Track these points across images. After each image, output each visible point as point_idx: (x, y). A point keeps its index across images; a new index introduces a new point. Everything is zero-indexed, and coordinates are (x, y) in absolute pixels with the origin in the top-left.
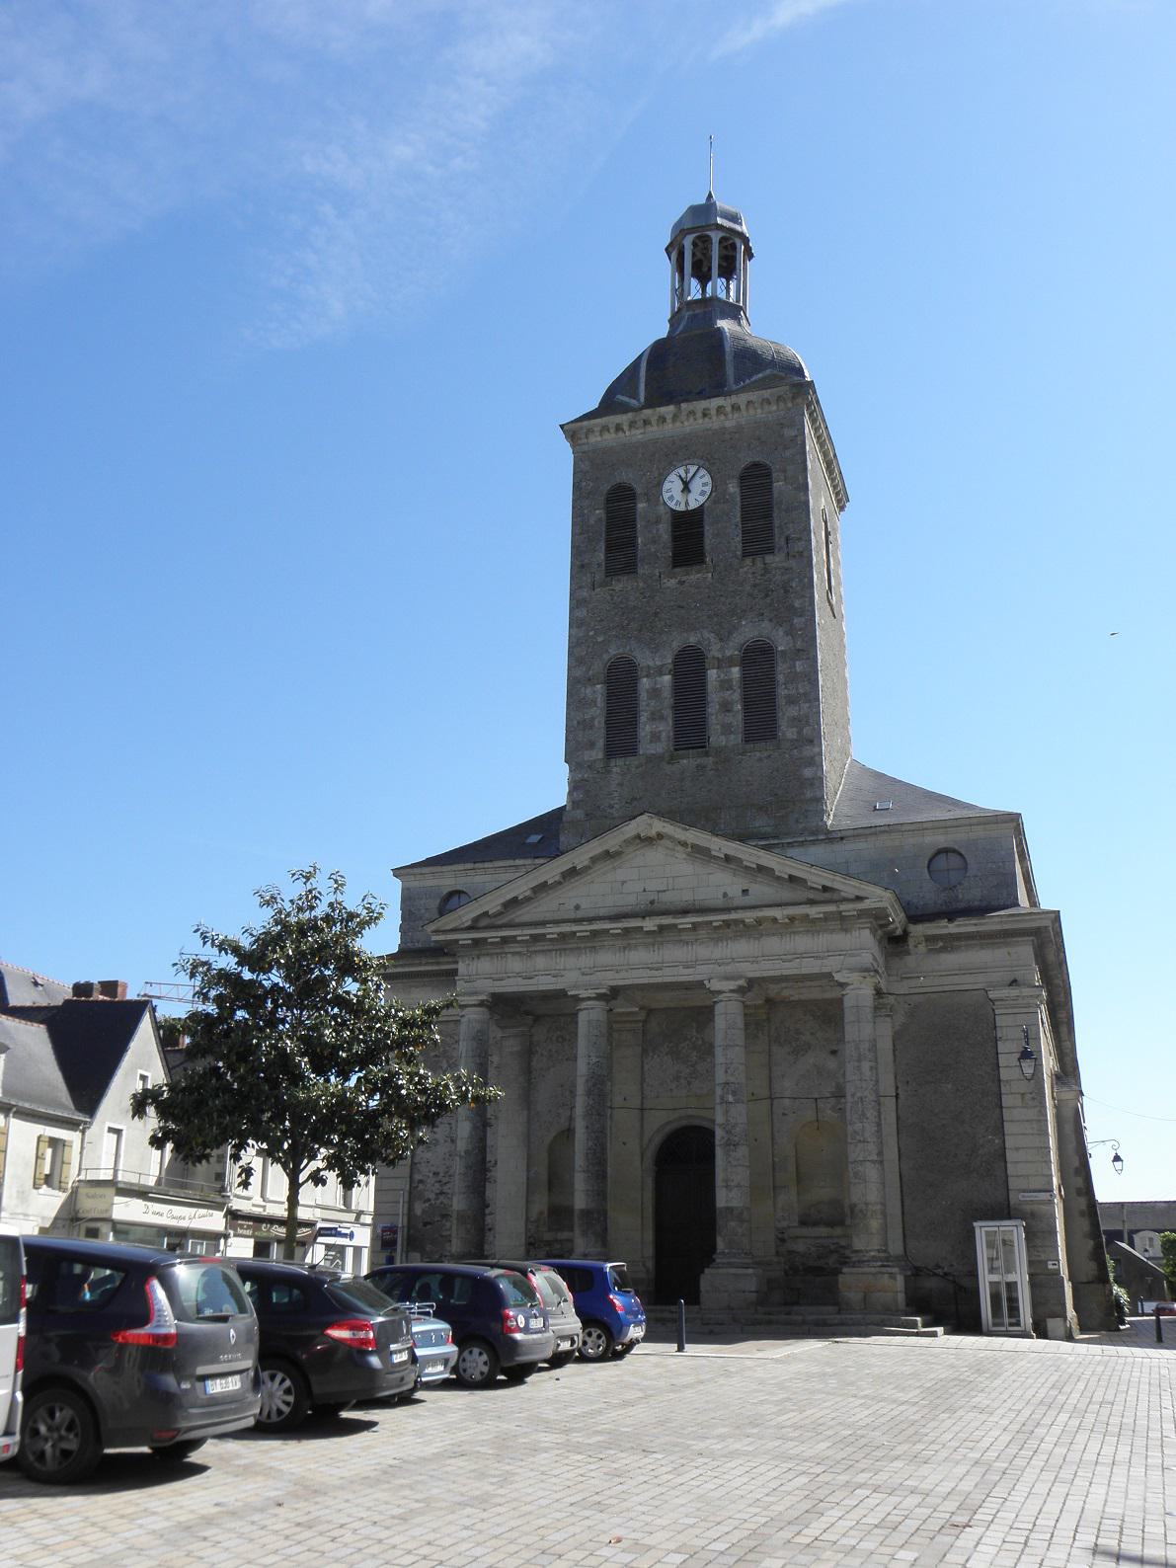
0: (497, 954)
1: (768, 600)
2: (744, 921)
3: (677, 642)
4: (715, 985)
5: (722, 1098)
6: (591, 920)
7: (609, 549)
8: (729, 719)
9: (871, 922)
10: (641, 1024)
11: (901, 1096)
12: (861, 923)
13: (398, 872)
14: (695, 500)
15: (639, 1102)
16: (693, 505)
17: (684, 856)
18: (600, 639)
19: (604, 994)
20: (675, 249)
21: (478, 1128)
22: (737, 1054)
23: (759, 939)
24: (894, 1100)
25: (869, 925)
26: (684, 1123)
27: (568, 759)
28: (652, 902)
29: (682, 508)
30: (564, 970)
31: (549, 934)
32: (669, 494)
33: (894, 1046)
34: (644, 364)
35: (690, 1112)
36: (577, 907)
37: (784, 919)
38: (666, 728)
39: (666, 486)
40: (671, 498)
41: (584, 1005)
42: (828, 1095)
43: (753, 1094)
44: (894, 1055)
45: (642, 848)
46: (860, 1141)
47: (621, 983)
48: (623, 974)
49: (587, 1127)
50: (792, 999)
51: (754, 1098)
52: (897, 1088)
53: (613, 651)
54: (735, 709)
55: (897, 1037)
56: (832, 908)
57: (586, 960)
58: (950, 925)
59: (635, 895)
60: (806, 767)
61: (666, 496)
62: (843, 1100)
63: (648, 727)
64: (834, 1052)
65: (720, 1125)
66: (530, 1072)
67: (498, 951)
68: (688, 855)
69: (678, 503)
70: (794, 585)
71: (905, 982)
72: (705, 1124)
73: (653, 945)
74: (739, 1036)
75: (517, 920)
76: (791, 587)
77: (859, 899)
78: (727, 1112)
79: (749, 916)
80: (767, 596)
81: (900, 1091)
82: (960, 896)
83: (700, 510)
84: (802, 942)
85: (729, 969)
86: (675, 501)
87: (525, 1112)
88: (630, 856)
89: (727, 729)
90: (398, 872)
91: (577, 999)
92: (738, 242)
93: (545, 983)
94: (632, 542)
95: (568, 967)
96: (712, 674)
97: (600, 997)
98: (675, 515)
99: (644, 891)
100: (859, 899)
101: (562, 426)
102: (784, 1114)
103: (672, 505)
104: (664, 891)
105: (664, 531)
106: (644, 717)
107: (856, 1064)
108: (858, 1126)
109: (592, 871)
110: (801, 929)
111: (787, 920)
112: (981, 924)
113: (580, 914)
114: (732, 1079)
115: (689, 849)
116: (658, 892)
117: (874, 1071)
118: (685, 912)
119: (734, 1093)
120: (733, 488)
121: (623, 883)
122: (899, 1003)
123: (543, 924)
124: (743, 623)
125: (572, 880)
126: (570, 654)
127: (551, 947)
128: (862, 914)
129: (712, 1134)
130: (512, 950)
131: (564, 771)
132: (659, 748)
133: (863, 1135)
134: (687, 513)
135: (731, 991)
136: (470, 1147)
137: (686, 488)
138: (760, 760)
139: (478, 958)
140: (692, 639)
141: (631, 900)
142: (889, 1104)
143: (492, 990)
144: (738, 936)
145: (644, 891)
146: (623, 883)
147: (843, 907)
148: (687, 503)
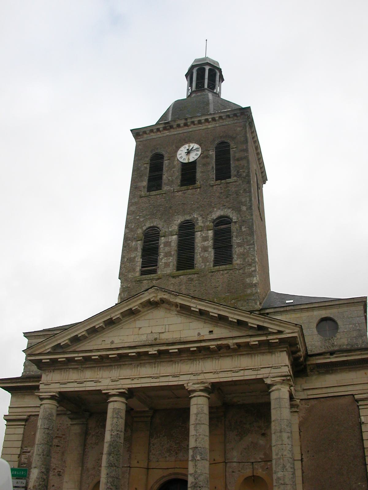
0: (64, 369)
1: (228, 199)
2: (209, 348)
3: (179, 220)
4: (190, 387)
5: (193, 457)
6: (118, 349)
7: (149, 181)
8: (206, 255)
9: (287, 347)
10: (149, 418)
11: (305, 460)
12: (281, 348)
13: (27, 335)
14: (193, 157)
15: (146, 464)
16: (191, 160)
17: (176, 313)
18: (141, 220)
19: (124, 393)
20: (189, 75)
21: (43, 472)
22: (205, 429)
23: (218, 359)
24: (300, 462)
25: (285, 349)
26: (173, 477)
27: (122, 276)
28: (156, 339)
29: (186, 161)
30: (102, 378)
31: (79, 334)
32: (180, 156)
33: (300, 430)
34: (171, 112)
35: (177, 471)
36: (112, 342)
37: (234, 345)
38: (173, 260)
39: (179, 152)
40: (181, 157)
41: (111, 399)
42: (260, 460)
43: (214, 460)
44: (300, 435)
45: (151, 309)
46: (282, 484)
47: (134, 386)
48: (135, 381)
49: (108, 474)
50: (239, 403)
51: (215, 462)
52: (302, 455)
53: (148, 225)
54: (210, 250)
55: (301, 425)
56: (263, 338)
57: (115, 373)
58: (331, 357)
59: (146, 336)
60: (247, 278)
61: (178, 157)
62: (269, 463)
63: (163, 261)
64: (263, 434)
65: (191, 474)
66: (85, 445)
67: (65, 367)
68: (178, 312)
69: (184, 159)
70: (241, 192)
71: (305, 392)
72: (186, 479)
73: (155, 364)
74: (205, 418)
75: (77, 350)
76: (240, 193)
77: (280, 332)
78: (196, 465)
79: (213, 345)
80: (227, 197)
81: (303, 457)
82: (336, 343)
83: (194, 163)
84: (245, 362)
85: (201, 377)
86: (183, 159)
87: (80, 468)
88: (144, 313)
89: (205, 260)
90: (27, 335)
91: (108, 395)
92: (217, 71)
93: (90, 386)
94: (160, 177)
95: (104, 377)
96: (198, 234)
97: (121, 394)
98: (183, 164)
99: (152, 333)
100: (280, 332)
101: (131, 130)
102: (233, 472)
103: (181, 160)
104: (163, 333)
105: (177, 173)
106: (161, 255)
107: (279, 434)
108: (280, 474)
109: (122, 322)
110: (245, 353)
111: (236, 346)
112: (349, 356)
113: (113, 346)
114: (198, 445)
115: (179, 309)
116: (160, 333)
117: (290, 439)
118: (173, 344)
119: (201, 454)
120: (212, 153)
121: (140, 328)
122: (302, 404)
123: (91, 351)
124: (215, 210)
125: (110, 327)
126: (127, 227)
127: (95, 365)
128: (282, 341)
129: (186, 482)
130: (72, 367)
131: (118, 284)
132: (168, 271)
133: (284, 480)
134: (189, 163)
135: (201, 390)
136: (37, 484)
137: (188, 152)
138: (222, 274)
139: (54, 371)
140: (188, 218)
141: (144, 338)
142: (298, 465)
143: (59, 390)
144: (205, 358)
145: (152, 333)
146: (140, 328)
147: (270, 337)
148: (189, 159)
